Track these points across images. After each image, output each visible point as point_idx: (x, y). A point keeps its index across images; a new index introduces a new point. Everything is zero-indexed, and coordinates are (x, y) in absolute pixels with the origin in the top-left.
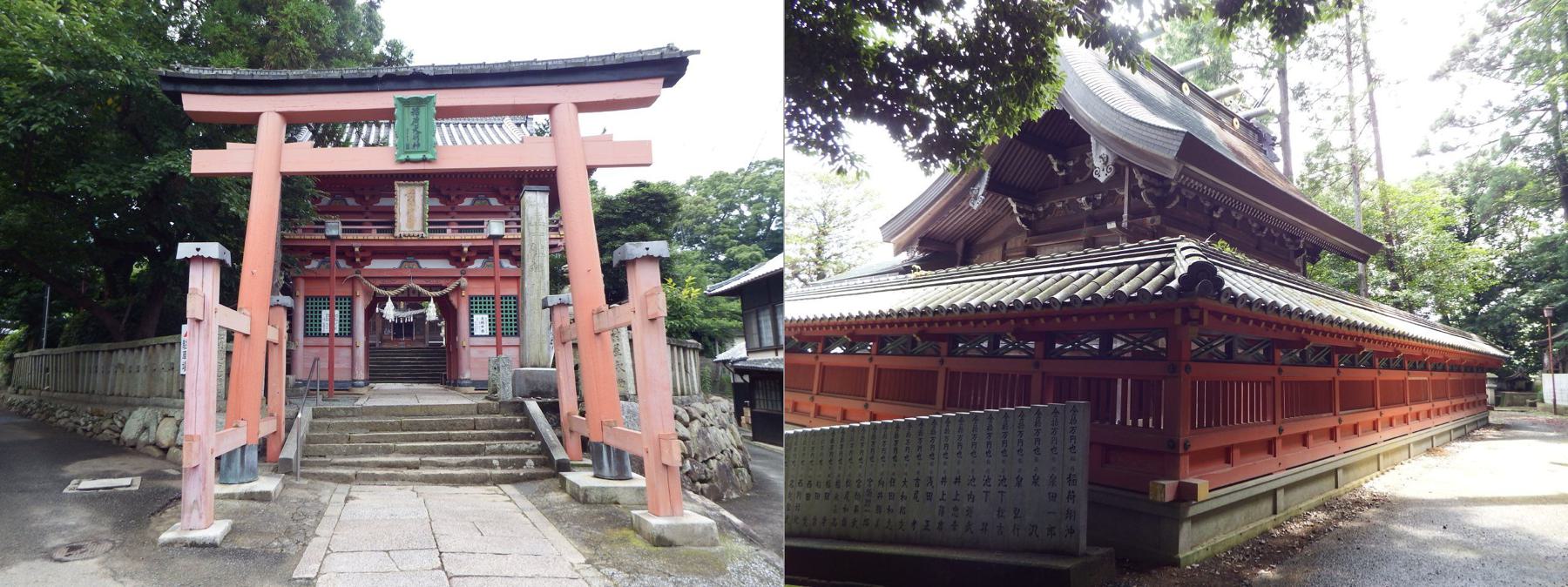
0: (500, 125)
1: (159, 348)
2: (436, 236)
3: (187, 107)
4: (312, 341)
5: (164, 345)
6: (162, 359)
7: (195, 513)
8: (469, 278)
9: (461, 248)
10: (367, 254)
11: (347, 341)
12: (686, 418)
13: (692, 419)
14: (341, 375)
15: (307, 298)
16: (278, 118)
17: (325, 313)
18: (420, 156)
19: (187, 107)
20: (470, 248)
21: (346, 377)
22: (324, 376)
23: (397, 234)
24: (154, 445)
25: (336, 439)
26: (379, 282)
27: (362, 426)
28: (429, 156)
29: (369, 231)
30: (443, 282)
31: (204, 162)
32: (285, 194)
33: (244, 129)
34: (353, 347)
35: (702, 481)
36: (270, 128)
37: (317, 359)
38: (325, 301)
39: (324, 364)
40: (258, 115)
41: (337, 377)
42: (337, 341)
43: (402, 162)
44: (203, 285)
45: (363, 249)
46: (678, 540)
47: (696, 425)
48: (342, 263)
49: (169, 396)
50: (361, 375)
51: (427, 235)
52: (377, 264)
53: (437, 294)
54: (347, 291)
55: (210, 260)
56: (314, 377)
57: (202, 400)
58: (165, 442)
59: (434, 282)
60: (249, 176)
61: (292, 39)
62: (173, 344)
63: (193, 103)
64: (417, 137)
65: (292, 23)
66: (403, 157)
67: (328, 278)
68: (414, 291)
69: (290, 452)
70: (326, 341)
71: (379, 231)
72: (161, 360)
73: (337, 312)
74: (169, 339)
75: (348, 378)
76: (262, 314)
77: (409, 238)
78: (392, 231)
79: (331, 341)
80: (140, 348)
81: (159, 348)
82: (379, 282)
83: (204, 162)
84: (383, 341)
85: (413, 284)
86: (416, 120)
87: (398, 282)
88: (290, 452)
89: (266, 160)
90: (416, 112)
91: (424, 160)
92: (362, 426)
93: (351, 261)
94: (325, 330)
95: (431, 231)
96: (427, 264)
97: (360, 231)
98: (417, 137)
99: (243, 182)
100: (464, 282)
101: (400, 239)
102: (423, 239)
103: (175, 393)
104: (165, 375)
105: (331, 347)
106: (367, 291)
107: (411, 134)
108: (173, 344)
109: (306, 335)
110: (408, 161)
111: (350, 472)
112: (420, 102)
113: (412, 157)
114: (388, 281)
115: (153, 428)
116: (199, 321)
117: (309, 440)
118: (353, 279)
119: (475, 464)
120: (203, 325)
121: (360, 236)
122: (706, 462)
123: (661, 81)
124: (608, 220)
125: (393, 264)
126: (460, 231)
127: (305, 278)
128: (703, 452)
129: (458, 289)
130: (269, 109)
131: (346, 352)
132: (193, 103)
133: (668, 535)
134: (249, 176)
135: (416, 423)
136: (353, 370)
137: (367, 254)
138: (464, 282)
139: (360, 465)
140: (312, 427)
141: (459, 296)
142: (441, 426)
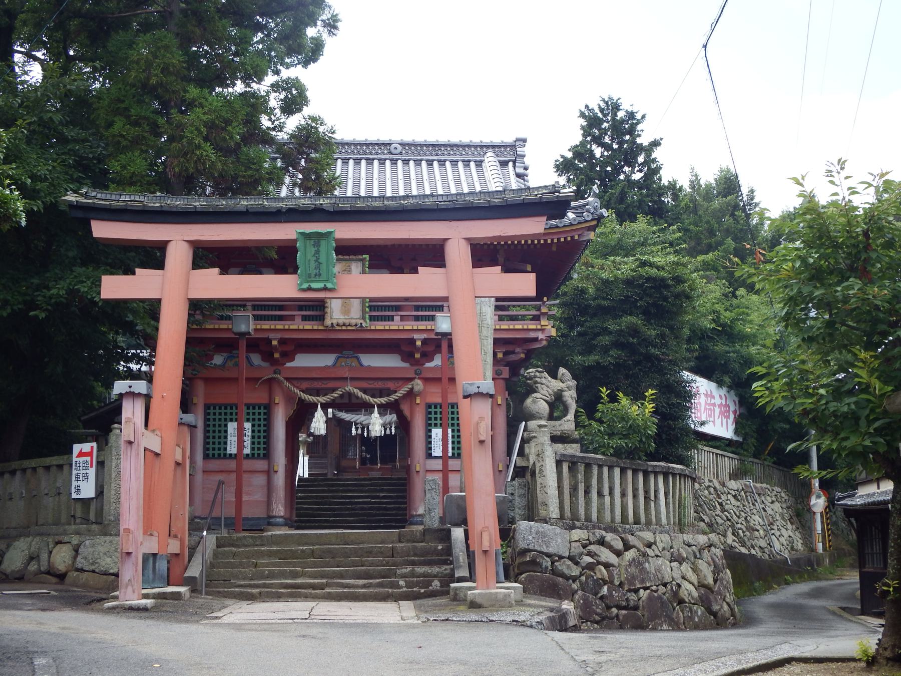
0: (479, 164)
1: (40, 471)
2: (380, 325)
3: (96, 234)
4: (215, 464)
5: (47, 468)
6: (44, 482)
7: (130, 589)
8: (426, 380)
9: (412, 341)
10: (290, 348)
11: (261, 464)
12: (619, 545)
13: (627, 547)
14: (253, 510)
15: (207, 407)
16: (186, 246)
17: (232, 427)
18: (320, 285)
19: (96, 234)
20: (425, 342)
21: (260, 513)
22: (231, 512)
23: (328, 322)
24: (48, 573)
25: (241, 565)
26: (305, 385)
27: (270, 554)
28: (329, 285)
29: (291, 318)
30: (391, 385)
31: (114, 287)
32: (190, 306)
33: (152, 256)
34: (269, 473)
35: (620, 608)
36: (178, 255)
37: (221, 483)
38: (230, 411)
39: (231, 497)
40: (166, 243)
41: (247, 513)
42: (247, 464)
43: (304, 290)
44: (132, 412)
45: (282, 341)
46: (485, 603)
47: (630, 555)
48: (256, 359)
49: (57, 523)
50: (279, 509)
51: (366, 324)
52: (304, 361)
53: (383, 400)
54: (259, 396)
55: (139, 394)
56: (214, 515)
57: (134, 503)
58: (61, 567)
59: (379, 385)
60: (159, 301)
61: (199, 147)
62: (60, 467)
63: (102, 230)
64: (318, 267)
65: (198, 129)
66: (305, 286)
67: (235, 380)
68: (350, 394)
69: (195, 570)
70: (232, 465)
71: (305, 318)
72: (43, 484)
73: (248, 425)
74: (54, 460)
75: (263, 515)
76: (171, 434)
77: (344, 327)
78: (321, 318)
79: (239, 465)
80: (13, 473)
81: (40, 471)
82: (305, 385)
83: (114, 287)
84: (340, 469)
85: (349, 388)
86: (317, 252)
87: (331, 385)
88: (195, 570)
89: (174, 287)
90: (317, 245)
91: (325, 289)
92: (270, 554)
93: (268, 356)
94: (232, 449)
95: (372, 318)
96: (372, 361)
97: (281, 318)
98: (318, 267)
99: (152, 308)
100: (418, 385)
101: (332, 329)
102: (362, 329)
103: (64, 519)
104: (49, 502)
105: (239, 472)
106: (289, 398)
107: (313, 264)
108: (60, 467)
109: (206, 457)
110: (310, 289)
111: (255, 591)
112: (319, 237)
113: (315, 285)
114: (318, 383)
115: (44, 556)
116: (130, 443)
117: (212, 566)
118: (270, 381)
119: (380, 585)
120: (134, 446)
121: (279, 325)
122: (636, 591)
123: (545, 218)
124: (600, 307)
125: (325, 360)
126: (417, 318)
127: (207, 380)
128: (632, 579)
129: (411, 394)
130: (179, 239)
131: (261, 480)
132: (102, 230)
133: (479, 600)
134: (159, 301)
135: (329, 551)
136: (269, 503)
137: (290, 348)
138: (418, 385)
139: (265, 586)
140: (215, 555)
141: (413, 404)
142: (355, 553)
